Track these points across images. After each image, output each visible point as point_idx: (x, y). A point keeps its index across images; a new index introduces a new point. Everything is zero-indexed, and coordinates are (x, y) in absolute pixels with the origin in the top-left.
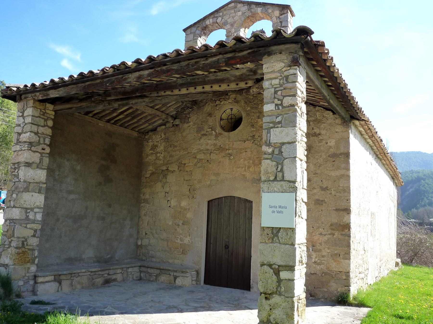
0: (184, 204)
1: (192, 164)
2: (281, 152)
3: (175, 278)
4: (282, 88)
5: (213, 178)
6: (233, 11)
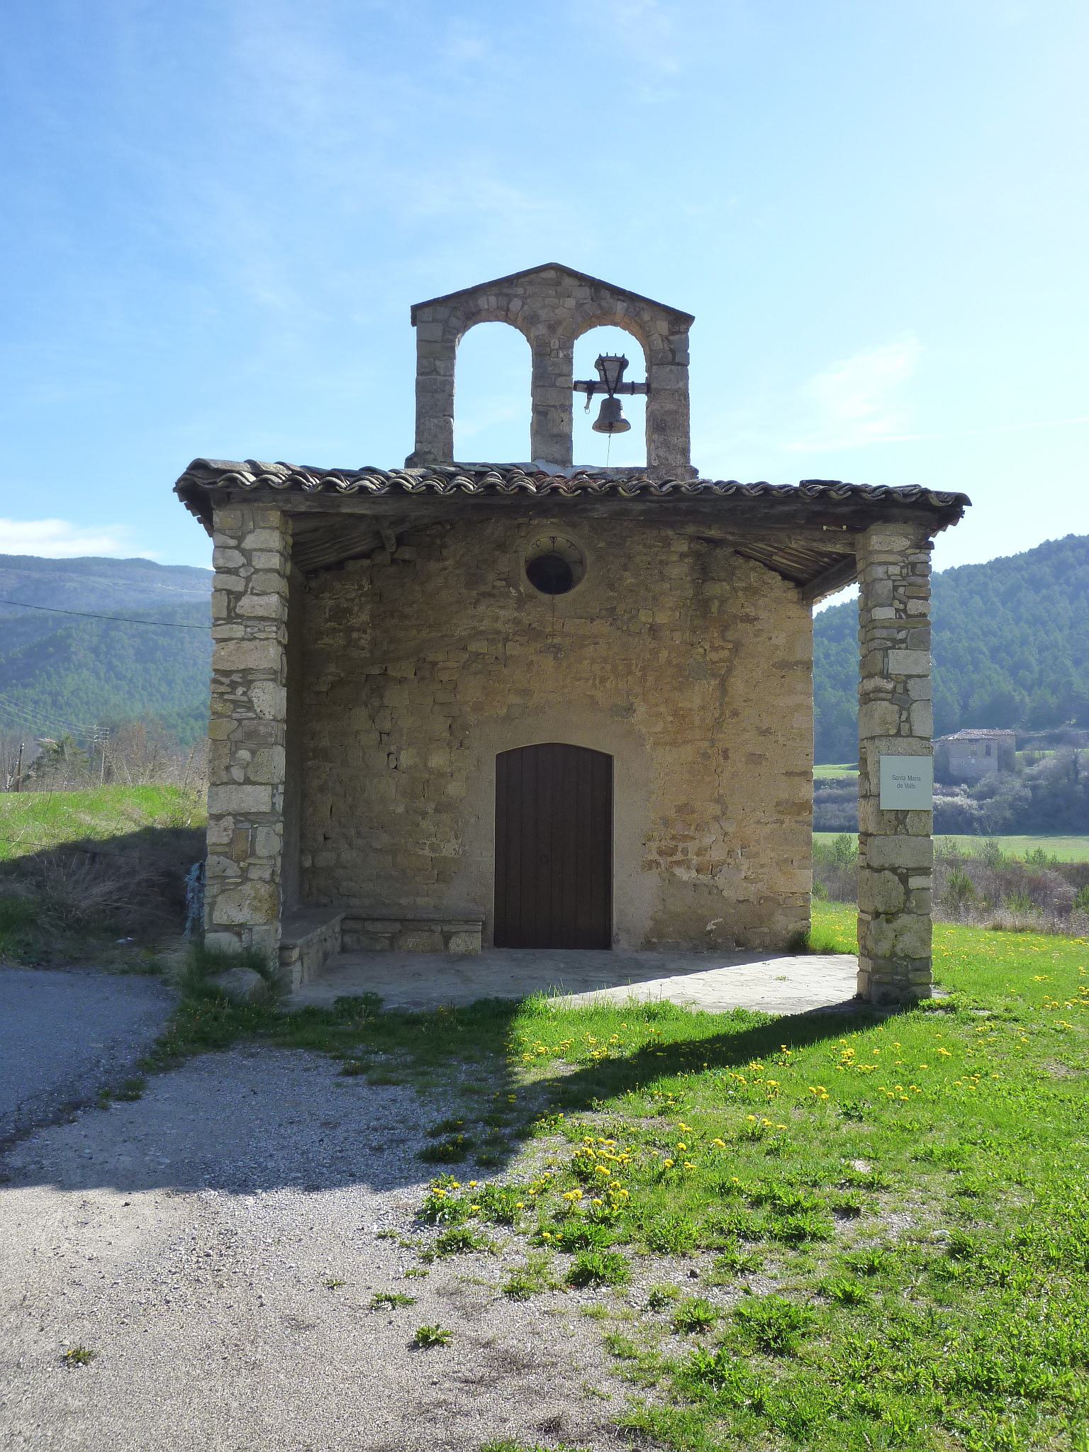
0: (437, 760)
1: (456, 665)
2: (906, 690)
3: (447, 937)
4: (904, 583)
5: (514, 699)
6: (552, 292)
